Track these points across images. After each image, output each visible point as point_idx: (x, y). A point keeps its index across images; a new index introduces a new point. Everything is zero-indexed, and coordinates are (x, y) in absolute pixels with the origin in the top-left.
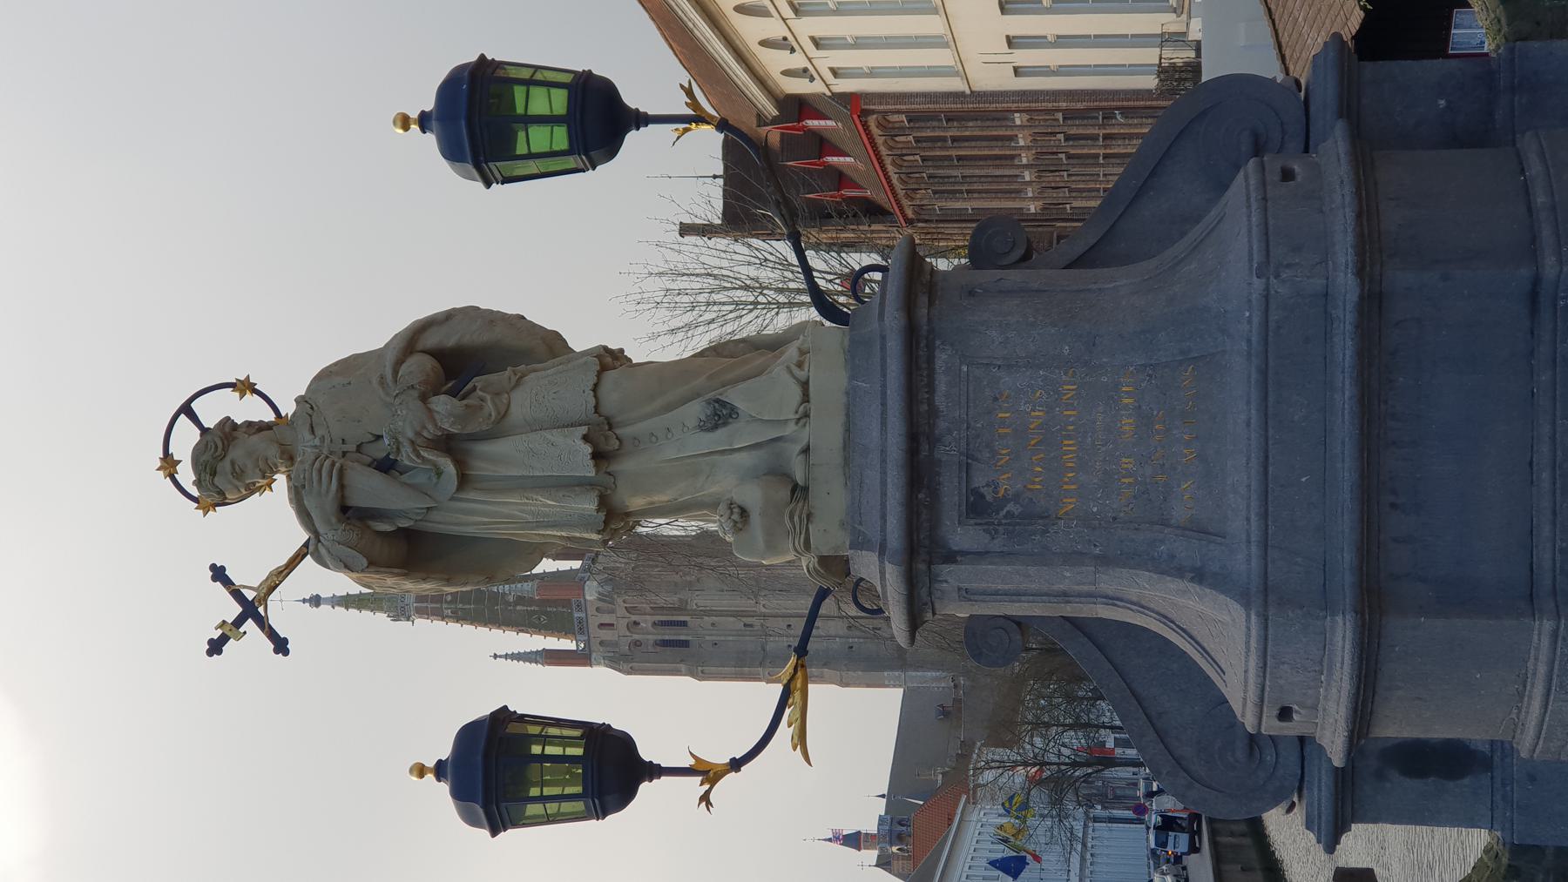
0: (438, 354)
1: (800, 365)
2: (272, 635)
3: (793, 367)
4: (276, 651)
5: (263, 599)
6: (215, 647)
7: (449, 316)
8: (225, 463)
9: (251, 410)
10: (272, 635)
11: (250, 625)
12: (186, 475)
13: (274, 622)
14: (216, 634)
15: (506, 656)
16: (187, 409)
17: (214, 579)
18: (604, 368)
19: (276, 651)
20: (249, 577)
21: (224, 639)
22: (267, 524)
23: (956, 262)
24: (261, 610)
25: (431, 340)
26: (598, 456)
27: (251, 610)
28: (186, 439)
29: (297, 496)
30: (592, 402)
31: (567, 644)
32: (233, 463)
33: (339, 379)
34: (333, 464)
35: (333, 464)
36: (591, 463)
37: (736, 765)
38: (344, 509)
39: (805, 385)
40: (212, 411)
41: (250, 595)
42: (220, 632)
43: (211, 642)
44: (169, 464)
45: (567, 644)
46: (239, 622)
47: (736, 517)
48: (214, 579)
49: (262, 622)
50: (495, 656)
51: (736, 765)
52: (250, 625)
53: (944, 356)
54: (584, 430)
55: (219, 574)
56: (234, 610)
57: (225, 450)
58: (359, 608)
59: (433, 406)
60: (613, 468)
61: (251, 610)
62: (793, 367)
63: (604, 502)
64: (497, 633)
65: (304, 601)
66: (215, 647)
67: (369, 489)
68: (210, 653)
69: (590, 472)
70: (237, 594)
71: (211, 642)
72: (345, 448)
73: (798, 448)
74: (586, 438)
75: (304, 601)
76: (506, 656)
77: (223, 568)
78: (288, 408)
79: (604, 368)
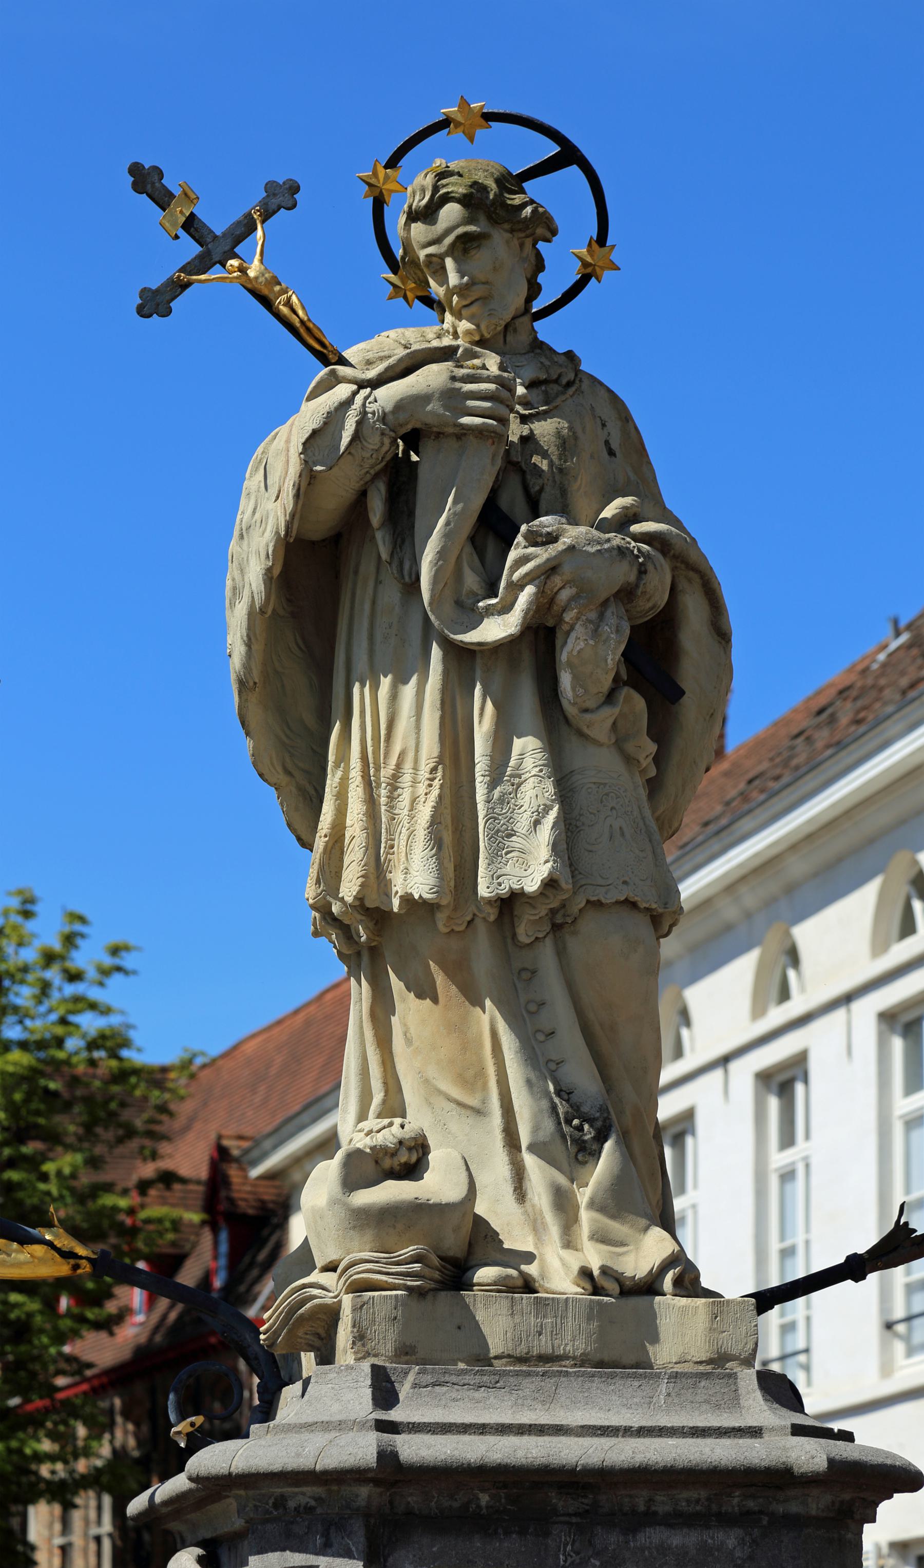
6: (146, 180)
7: (723, 636)
11: (190, 249)
14: (171, 182)
21: (163, 199)
25: (693, 609)
30: (610, 897)
36: (504, 890)
37: (602, 238)
38: (413, 439)
42: (177, 192)
46: (191, 225)
48: (271, 188)
49: (202, 264)
51: (602, 238)
52: (190, 249)
53: (731, 1543)
60: (481, 929)
66: (146, 180)
74: (550, 884)
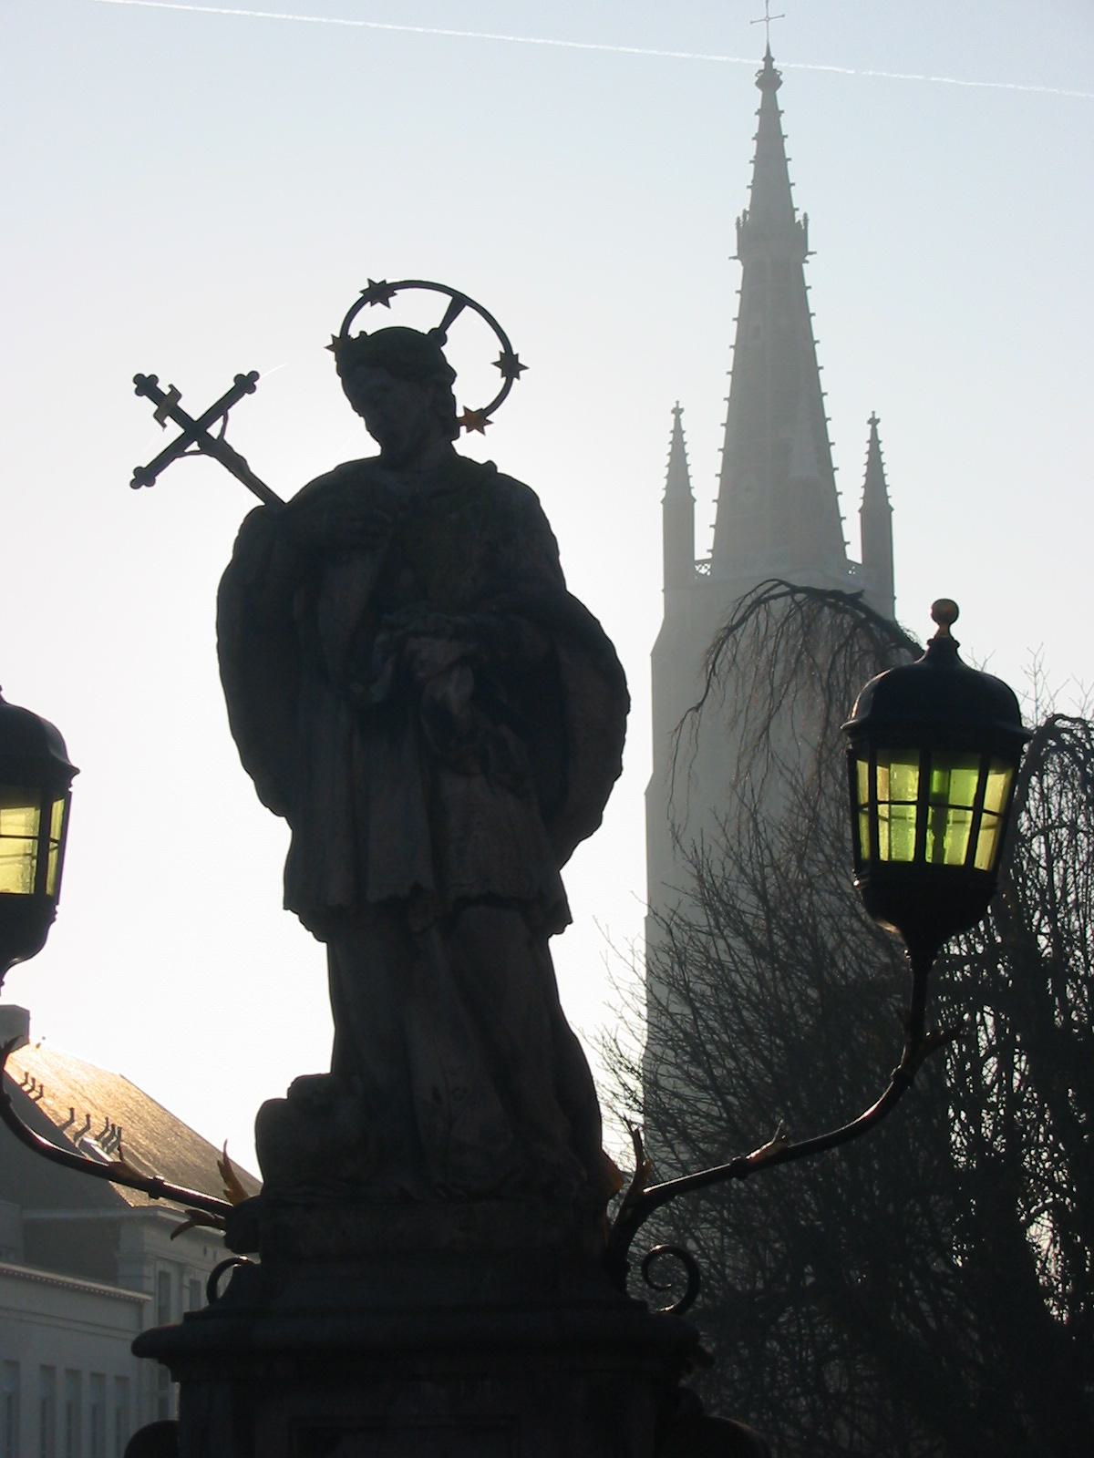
4: (138, 471)
6: (146, 385)
8: (395, 374)
9: (470, 391)
12: (372, 320)
16: (459, 302)
17: (239, 378)
19: (138, 471)
20: (239, 430)
22: (311, 435)
23: (721, 909)
24: (194, 446)
27: (199, 436)
28: (416, 312)
29: (350, 474)
31: (704, 543)
40: (470, 355)
41: (214, 430)
43: (154, 379)
44: (379, 293)
45: (704, 543)
46: (181, 417)
48: (239, 378)
52: (174, 430)
55: (245, 384)
56: (194, 407)
58: (756, 186)
64: (719, 437)
65: (769, 59)
66: (146, 385)
68: (139, 379)
70: (220, 409)
71: (154, 379)
75: (769, 59)
77: (252, 389)
78: (468, 445)
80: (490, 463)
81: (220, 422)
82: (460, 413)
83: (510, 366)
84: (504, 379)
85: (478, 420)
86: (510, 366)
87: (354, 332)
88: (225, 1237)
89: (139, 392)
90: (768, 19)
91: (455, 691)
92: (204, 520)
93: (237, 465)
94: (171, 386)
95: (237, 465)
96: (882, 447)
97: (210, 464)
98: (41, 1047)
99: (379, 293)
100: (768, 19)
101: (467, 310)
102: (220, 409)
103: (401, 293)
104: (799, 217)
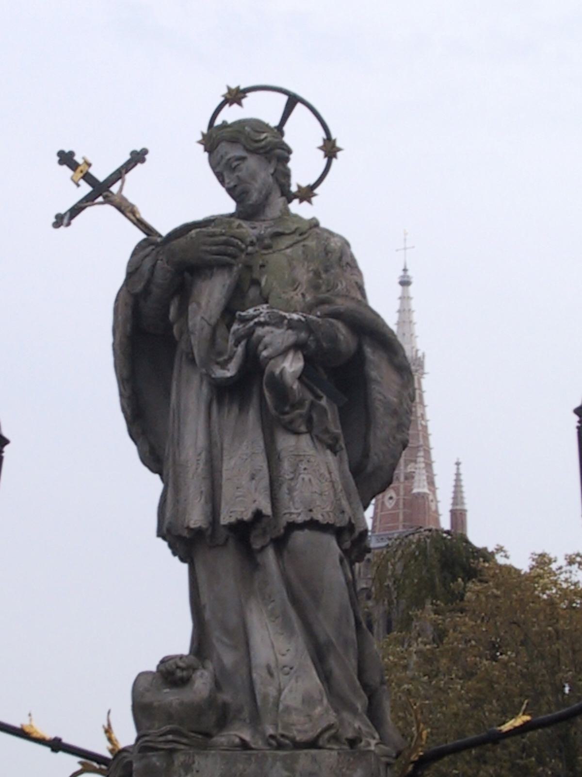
0: (359, 359)
1: (335, 738)
2: (75, 211)
3: (333, 731)
5: (108, 200)
6: (66, 159)
8: (246, 152)
9: (303, 167)
10: (75, 211)
11: (86, 189)
12: (231, 115)
13: (89, 212)
14: (78, 159)
15: (458, 475)
16: (293, 100)
18: (339, 532)
20: (132, 188)
22: (186, 194)
24: (100, 199)
26: (242, 530)
27: (100, 191)
28: (264, 109)
30: (300, 519)
32: (243, 159)
33: (333, 260)
34: (234, 257)
35: (234, 257)
39: (313, 744)
40: (302, 138)
41: (115, 189)
43: (72, 154)
44: (235, 96)
46: (88, 178)
47: (179, 674)
50: (458, 464)
52: (86, 189)
54: (267, 510)
56: (101, 174)
57: (254, 152)
59: (290, 356)
60: (231, 543)
61: (100, 191)
62: (333, 731)
63: (198, 533)
65: (405, 270)
66: (66, 159)
67: (211, 294)
69: (225, 519)
70: (119, 175)
71: (72, 154)
72: (256, 269)
73: (247, 737)
74: (258, 515)
75: (405, 270)
76: (458, 475)
77: (143, 160)
79: (339, 532)
80: (314, 219)
81: (119, 183)
82: (294, 189)
83: (330, 149)
84: (326, 159)
85: (307, 194)
86: (330, 149)
87: (218, 122)
88: (439, 531)
89: (61, 162)
90: (405, 249)
91: (291, 366)
92: (106, 249)
93: (126, 209)
94: (83, 158)
95: (126, 209)
96: (462, 477)
97: (109, 210)
98: (287, 649)
99: (235, 96)
100: (405, 249)
101: (299, 107)
102: (119, 175)
103: (251, 95)
104: (420, 354)
